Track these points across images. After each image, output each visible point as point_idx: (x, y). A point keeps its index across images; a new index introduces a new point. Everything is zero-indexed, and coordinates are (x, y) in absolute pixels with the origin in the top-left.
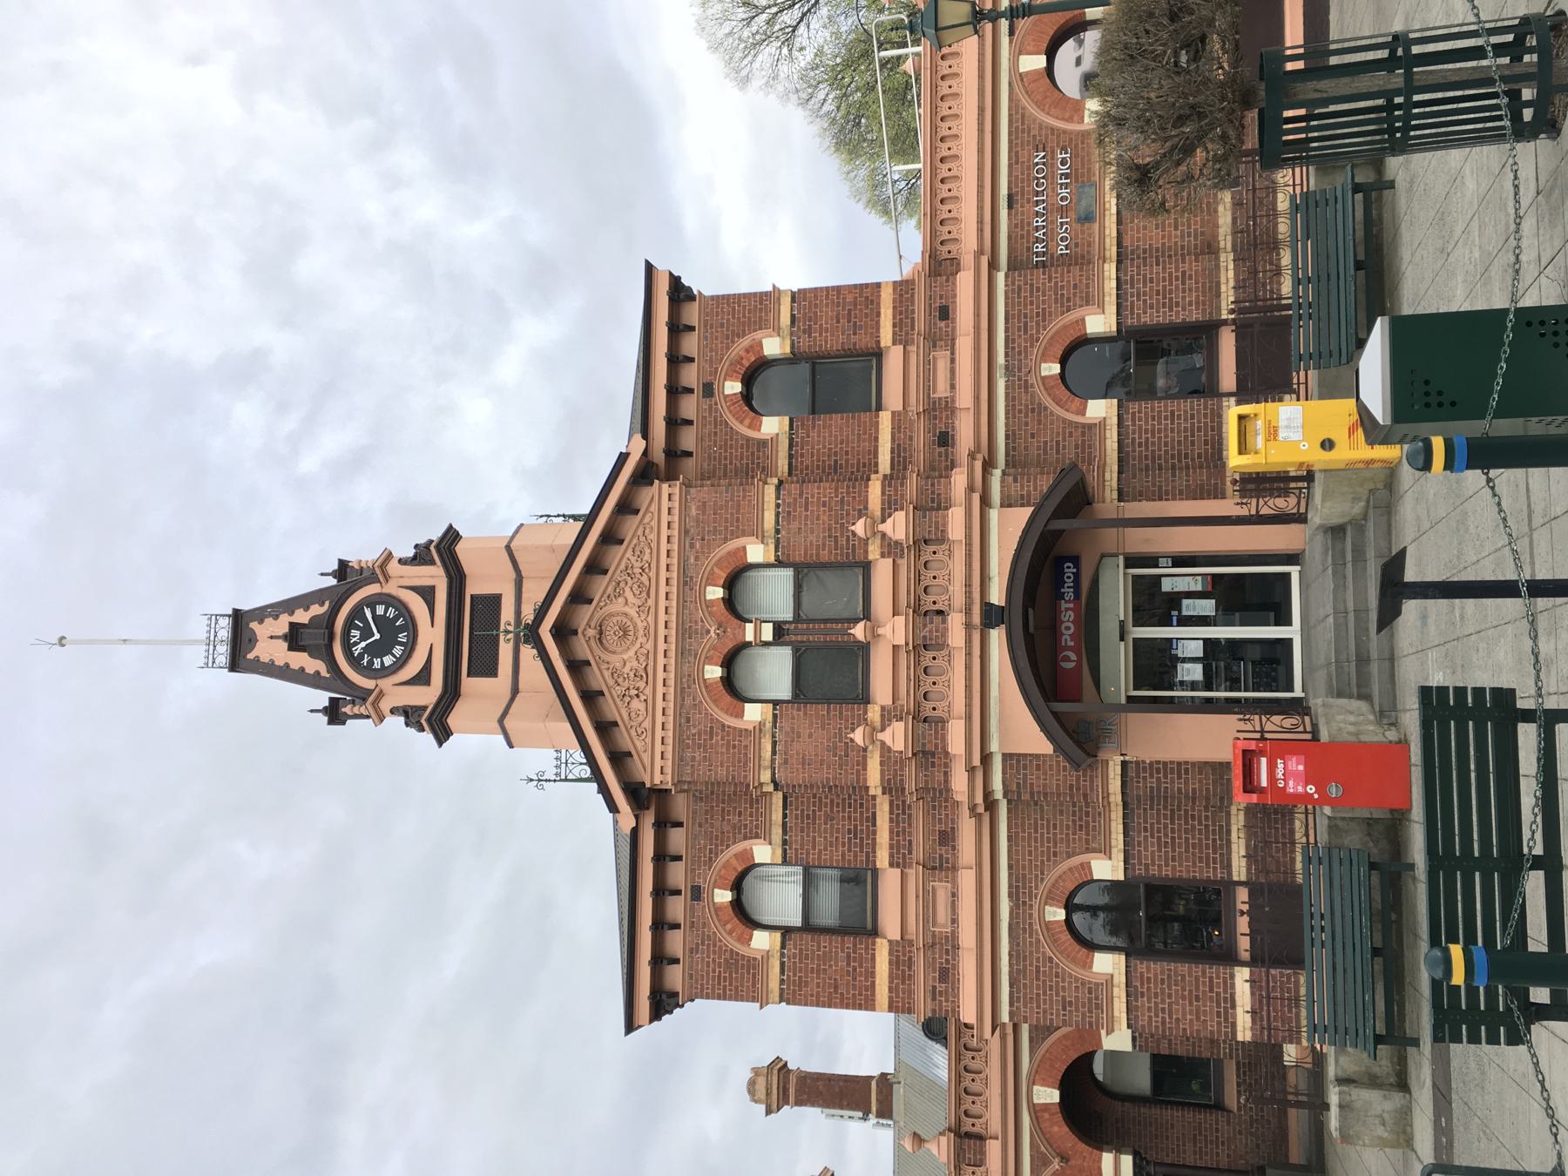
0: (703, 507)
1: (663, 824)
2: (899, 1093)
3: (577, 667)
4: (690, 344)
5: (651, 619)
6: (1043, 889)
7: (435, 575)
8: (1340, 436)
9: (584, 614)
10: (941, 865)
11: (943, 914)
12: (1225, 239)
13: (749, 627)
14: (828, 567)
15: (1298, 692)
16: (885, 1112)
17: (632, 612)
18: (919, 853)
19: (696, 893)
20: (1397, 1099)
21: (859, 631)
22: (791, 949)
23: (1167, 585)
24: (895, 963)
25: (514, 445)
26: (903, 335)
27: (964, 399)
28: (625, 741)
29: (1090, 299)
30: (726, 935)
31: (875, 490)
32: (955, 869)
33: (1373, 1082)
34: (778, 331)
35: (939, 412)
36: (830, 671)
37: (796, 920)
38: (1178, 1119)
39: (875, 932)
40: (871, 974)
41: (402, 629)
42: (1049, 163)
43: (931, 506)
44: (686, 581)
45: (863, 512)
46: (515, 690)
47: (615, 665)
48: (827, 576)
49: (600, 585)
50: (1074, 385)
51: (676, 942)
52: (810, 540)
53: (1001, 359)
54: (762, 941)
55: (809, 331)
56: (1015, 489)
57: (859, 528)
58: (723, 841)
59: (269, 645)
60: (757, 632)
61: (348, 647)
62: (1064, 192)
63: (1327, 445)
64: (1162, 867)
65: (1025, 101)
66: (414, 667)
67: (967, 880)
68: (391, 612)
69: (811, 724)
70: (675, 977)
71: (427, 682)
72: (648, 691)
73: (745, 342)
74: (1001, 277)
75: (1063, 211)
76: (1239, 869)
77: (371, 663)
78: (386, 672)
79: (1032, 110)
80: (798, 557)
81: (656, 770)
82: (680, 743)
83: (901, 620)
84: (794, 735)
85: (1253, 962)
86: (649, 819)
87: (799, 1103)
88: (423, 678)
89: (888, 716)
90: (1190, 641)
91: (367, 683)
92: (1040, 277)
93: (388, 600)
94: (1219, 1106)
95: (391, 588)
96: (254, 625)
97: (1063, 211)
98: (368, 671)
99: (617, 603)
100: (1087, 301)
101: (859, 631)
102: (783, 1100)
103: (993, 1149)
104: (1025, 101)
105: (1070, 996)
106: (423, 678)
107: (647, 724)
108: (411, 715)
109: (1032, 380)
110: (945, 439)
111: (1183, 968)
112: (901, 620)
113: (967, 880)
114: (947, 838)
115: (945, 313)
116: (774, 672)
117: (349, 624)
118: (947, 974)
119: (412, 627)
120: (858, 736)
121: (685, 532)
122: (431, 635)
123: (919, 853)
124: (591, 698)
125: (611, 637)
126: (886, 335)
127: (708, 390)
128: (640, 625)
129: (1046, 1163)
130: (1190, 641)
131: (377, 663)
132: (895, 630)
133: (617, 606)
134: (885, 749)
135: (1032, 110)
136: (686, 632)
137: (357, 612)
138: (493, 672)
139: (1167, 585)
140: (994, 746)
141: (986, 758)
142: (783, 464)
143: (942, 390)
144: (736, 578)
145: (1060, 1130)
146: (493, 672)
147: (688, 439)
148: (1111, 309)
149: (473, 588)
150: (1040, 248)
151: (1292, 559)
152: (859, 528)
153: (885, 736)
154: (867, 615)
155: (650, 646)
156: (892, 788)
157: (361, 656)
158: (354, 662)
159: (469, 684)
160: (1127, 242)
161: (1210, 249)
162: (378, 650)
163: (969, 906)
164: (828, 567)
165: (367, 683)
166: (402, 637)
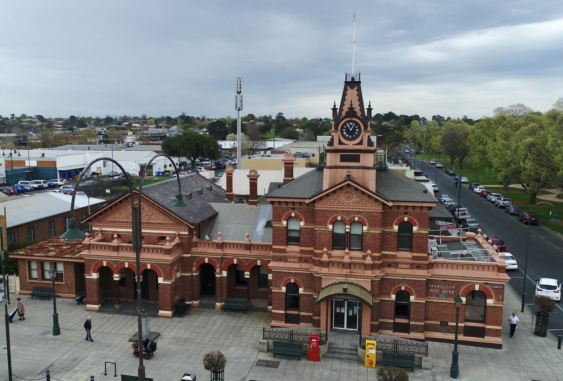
0: (376, 216)
3: (341, 188)
4: (418, 210)
5: (351, 205)
6: (296, 279)
8: (369, 358)
11: (291, 260)
12: (428, 322)
14: (361, 242)
15: (334, 328)
17: (353, 200)
19: (293, 209)
20: (266, 351)
23: (355, 307)
26: (414, 258)
27: (398, 271)
32: (300, 262)
33: (268, 346)
34: (418, 230)
35: (396, 265)
36: (339, 241)
37: (289, 228)
41: (352, 136)
42: (452, 289)
44: (359, 213)
45: (372, 252)
47: (342, 197)
48: (360, 241)
52: (367, 240)
53: (406, 278)
54: (285, 223)
55: (418, 237)
56: (376, 283)
58: (304, 215)
59: (352, 93)
60: (348, 228)
61: (348, 122)
62: (445, 292)
63: (368, 356)
64: (301, 300)
65: (468, 285)
67: (297, 265)
68: (356, 133)
69: (328, 239)
70: (276, 205)
72: (335, 204)
75: (440, 291)
76: (302, 313)
77: (344, 128)
78: (342, 132)
79: (465, 286)
80: (364, 238)
81: (318, 207)
82: (323, 211)
84: (326, 235)
85: (286, 314)
88: (340, 143)
90: (344, 310)
91: (339, 128)
92: (424, 287)
93: (360, 132)
94: (259, 287)
95: (362, 133)
96: (356, 88)
97: (440, 291)
98: (342, 128)
99: (355, 198)
102: (251, 179)
104: (468, 285)
105: (278, 282)
106: (340, 143)
107: (328, 203)
109: (401, 285)
111: (284, 302)
116: (340, 230)
117: (354, 122)
119: (353, 139)
121: (371, 212)
122: (350, 145)
124: (334, 192)
125: (348, 195)
128: (350, 201)
129: (247, 262)
130: (344, 310)
131: (344, 130)
132: (347, 260)
135: (465, 286)
136: (348, 212)
137: (357, 124)
139: (355, 307)
143: (400, 266)
145: (253, 265)
148: (415, 301)
149: (362, 155)
150: (432, 286)
151: (360, 330)
153: (325, 255)
155: (345, 204)
157: (346, 126)
158: (345, 124)
159: (338, 155)
164: (361, 242)
165: (339, 128)
166: (350, 137)
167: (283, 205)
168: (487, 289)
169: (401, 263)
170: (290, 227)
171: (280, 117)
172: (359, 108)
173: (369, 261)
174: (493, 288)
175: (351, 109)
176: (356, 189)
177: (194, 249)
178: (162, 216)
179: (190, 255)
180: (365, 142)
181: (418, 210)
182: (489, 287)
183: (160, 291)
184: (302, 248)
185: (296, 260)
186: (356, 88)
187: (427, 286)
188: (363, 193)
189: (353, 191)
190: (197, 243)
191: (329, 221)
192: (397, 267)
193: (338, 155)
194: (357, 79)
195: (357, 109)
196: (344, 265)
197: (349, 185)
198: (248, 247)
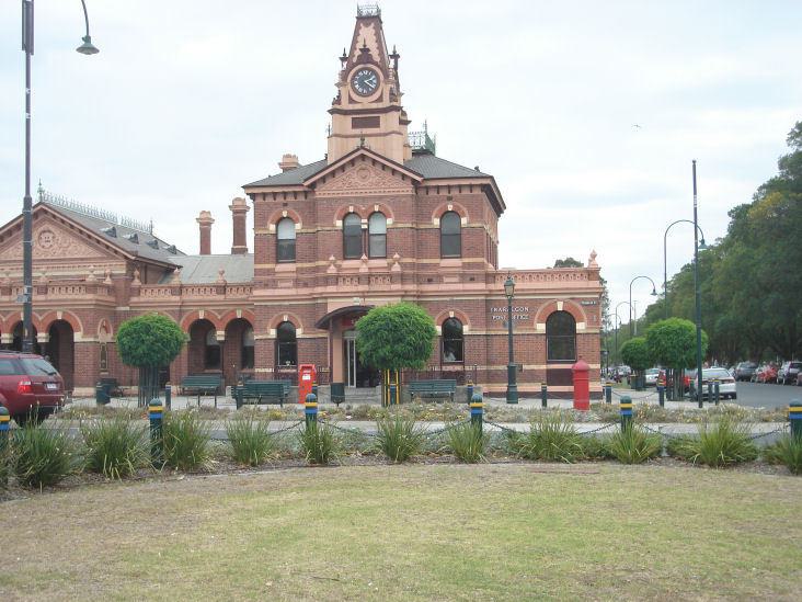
0: (404, 202)
1: (306, 193)
2: (241, 256)
3: (352, 162)
4: (466, 192)
7: (386, 103)
9: (370, 164)
10: (297, 283)
11: (283, 285)
12: (493, 368)
13: (366, 221)
16: (234, 251)
18: (300, 276)
21: (364, 257)
22: (271, 237)
24: (268, 270)
25: (448, 117)
27: (442, 287)
28: (328, 181)
29: (86, 333)
30: (273, 216)
31: (409, 260)
34: (394, 223)
35: (439, 278)
38: (238, 357)
39: (277, 262)
40: (265, 263)
43: (403, 278)
44: (381, 198)
45: (402, 256)
46: (347, 137)
49: (379, 168)
50: (280, 327)
51: (270, 199)
54: (272, 227)
55: (468, 233)
57: (397, 256)
58: (302, 213)
59: (368, 33)
61: (361, 70)
66: (355, 97)
67: (293, 292)
71: (350, 102)
73: (466, 212)
74: (483, 298)
81: (321, 193)
83: (367, 270)
86: (306, 189)
87: (234, 218)
88: (351, 101)
89: (339, 268)
92: (483, 310)
94: (243, 367)
98: (353, 79)
100: (473, 326)
101: (364, 257)
102: (235, 212)
103: (222, 297)
104: (546, 304)
106: (351, 101)
108: (338, 101)
110: (430, 281)
112: (367, 270)
113: (293, 292)
114: (306, 285)
115: (472, 280)
117: (369, 69)
118: (266, 286)
120: (332, 258)
121: (397, 196)
122: (366, 103)
123: (300, 276)
125: (364, 173)
126: (466, 260)
127: (450, 199)
132: (364, 269)
133: (373, 174)
134: (327, 267)
135: (543, 306)
137: (374, 72)
138: (354, 126)
140: (329, 300)
141: (326, 298)
142: (422, 227)
144: (383, 214)
146: (354, 126)
147: (433, 193)
149: (382, 116)
152: (397, 256)
153: (332, 267)
154: (370, 258)
156: (317, 269)
159: (349, 119)
160: (497, 338)
161: (489, 362)
162: (362, 84)
163: (286, 290)
167: (270, 199)
168: (573, 306)
169: (282, 280)
170: (282, 236)
171: (289, 165)
172: (376, 45)
173: (396, 268)
174: (583, 305)
175: (365, 50)
176: (374, 162)
177: (134, 299)
178: (84, 247)
179: (128, 308)
180: (386, 97)
181: (466, 192)
182: (577, 305)
183: (77, 355)
184: (299, 265)
185: (290, 284)
186: (373, 25)
187: (488, 311)
188: (384, 167)
189: (368, 164)
190: (139, 290)
191: (336, 215)
192: (441, 282)
193: (349, 119)
194: (374, 13)
195: (374, 53)
196: (359, 278)
197: (363, 157)
198: (222, 288)
